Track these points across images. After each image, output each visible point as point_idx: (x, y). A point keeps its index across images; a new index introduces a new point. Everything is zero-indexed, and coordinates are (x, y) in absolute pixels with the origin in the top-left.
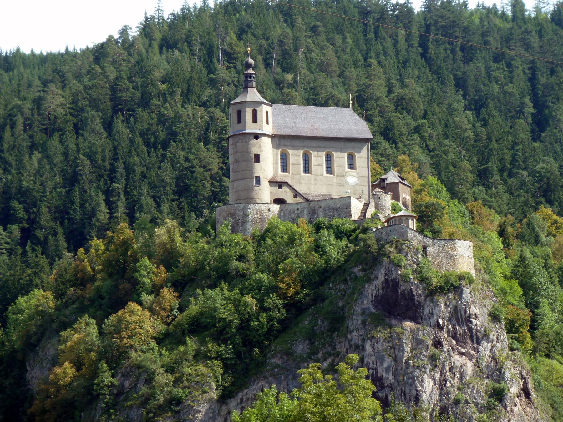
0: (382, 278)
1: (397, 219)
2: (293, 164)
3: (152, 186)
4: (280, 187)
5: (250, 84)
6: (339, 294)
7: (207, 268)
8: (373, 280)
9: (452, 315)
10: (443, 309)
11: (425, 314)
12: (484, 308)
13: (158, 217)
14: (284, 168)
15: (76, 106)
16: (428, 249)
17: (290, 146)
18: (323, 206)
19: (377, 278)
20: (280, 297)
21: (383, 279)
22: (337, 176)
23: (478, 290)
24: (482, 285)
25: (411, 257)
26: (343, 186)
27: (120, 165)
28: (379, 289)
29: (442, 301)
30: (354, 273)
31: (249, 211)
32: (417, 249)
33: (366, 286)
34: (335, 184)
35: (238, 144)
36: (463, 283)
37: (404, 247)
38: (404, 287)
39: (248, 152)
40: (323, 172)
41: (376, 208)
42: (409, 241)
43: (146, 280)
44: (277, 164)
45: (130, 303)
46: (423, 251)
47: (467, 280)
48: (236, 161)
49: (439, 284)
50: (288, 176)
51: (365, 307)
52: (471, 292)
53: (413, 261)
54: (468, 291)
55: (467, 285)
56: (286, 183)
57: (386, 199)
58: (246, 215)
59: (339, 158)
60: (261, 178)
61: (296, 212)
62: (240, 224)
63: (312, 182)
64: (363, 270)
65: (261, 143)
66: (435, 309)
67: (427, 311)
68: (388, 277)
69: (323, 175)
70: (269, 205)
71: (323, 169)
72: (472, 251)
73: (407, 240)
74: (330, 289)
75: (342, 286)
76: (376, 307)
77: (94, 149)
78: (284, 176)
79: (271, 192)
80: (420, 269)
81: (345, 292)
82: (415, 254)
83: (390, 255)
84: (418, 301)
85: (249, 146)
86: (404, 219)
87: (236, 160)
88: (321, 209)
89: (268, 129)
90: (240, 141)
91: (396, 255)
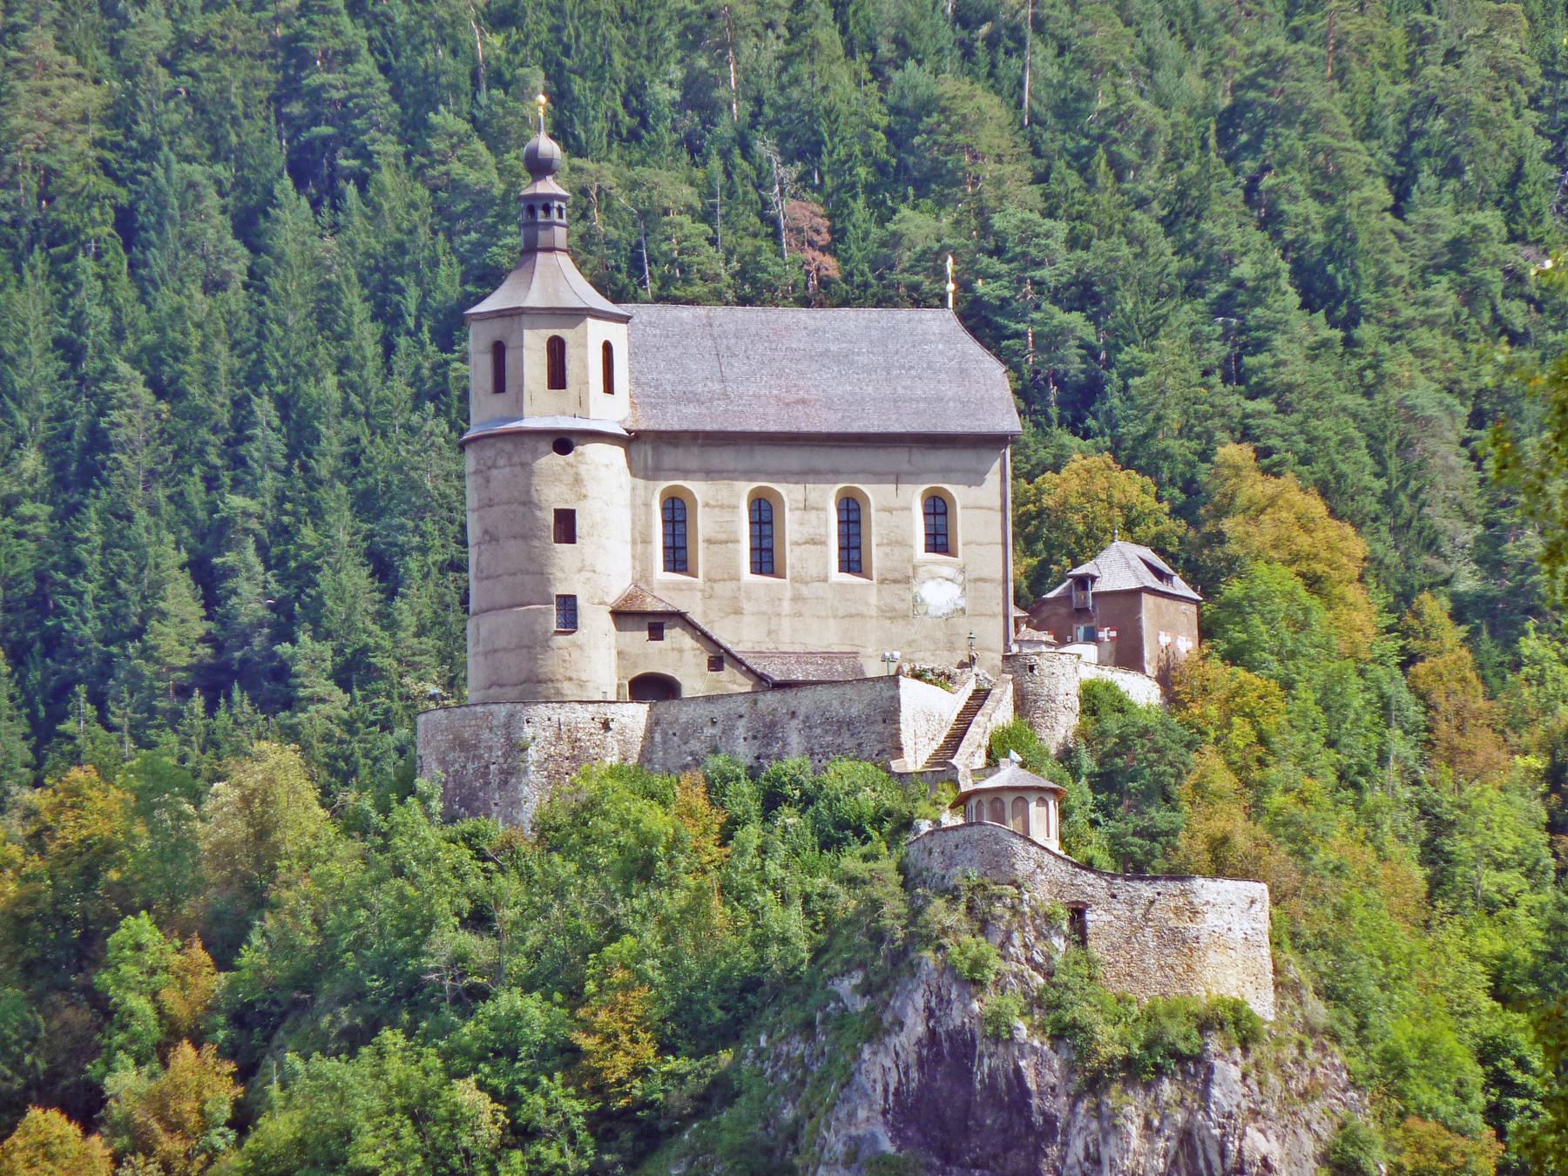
0: (916, 1026)
1: (985, 799)
2: (709, 541)
3: (366, 504)
4: (656, 633)
5: (543, 236)
6: (785, 1076)
7: (350, 961)
8: (888, 1032)
9: (1175, 1162)
10: (1135, 1143)
11: (1069, 1161)
12: (1302, 1131)
13: (378, 647)
14: (678, 558)
15: (129, 134)
16: (1089, 916)
17: (700, 471)
18: (802, 712)
19: (901, 1025)
20: (578, 1086)
21: (920, 1029)
22: (882, 581)
23: (1279, 1064)
24: (1301, 1046)
25: (1025, 946)
26: (906, 617)
27: (264, 408)
28: (907, 1067)
29: (1131, 1107)
30: (838, 999)
31: (528, 731)
32: (1048, 917)
33: (866, 1055)
34: (874, 612)
35: (494, 472)
36: (1214, 1043)
37: (998, 909)
38: (995, 1062)
39: (529, 503)
40: (826, 566)
41: (1016, 708)
42: (1018, 887)
43: (138, 1003)
44: (646, 541)
45: (34, 1113)
46: (1072, 920)
47: (1231, 1030)
48: (490, 536)
49: (1120, 1051)
50: (691, 588)
51: (861, 1132)
52: (1244, 1076)
53: (1030, 960)
54: (1235, 1073)
55: (1230, 1049)
56: (680, 618)
57: (1058, 671)
58: (516, 748)
59: (890, 511)
60: (580, 602)
61: (709, 731)
62: (494, 780)
63: (786, 606)
64: (866, 989)
65: (582, 469)
66: (1106, 1142)
67: (1077, 1149)
68: (938, 1021)
69: (825, 580)
70: (604, 708)
71: (826, 556)
72: (1264, 916)
73: (1013, 883)
74: (759, 1053)
75: (798, 1047)
76: (897, 1135)
77: (174, 335)
78: (677, 588)
79: (620, 654)
80: (1052, 994)
81: (807, 1070)
82: (1041, 936)
83: (945, 941)
84: (1043, 1113)
85: (535, 480)
86: (1008, 799)
87: (486, 532)
88: (794, 723)
89: (612, 413)
90: (501, 462)
91: (967, 939)
